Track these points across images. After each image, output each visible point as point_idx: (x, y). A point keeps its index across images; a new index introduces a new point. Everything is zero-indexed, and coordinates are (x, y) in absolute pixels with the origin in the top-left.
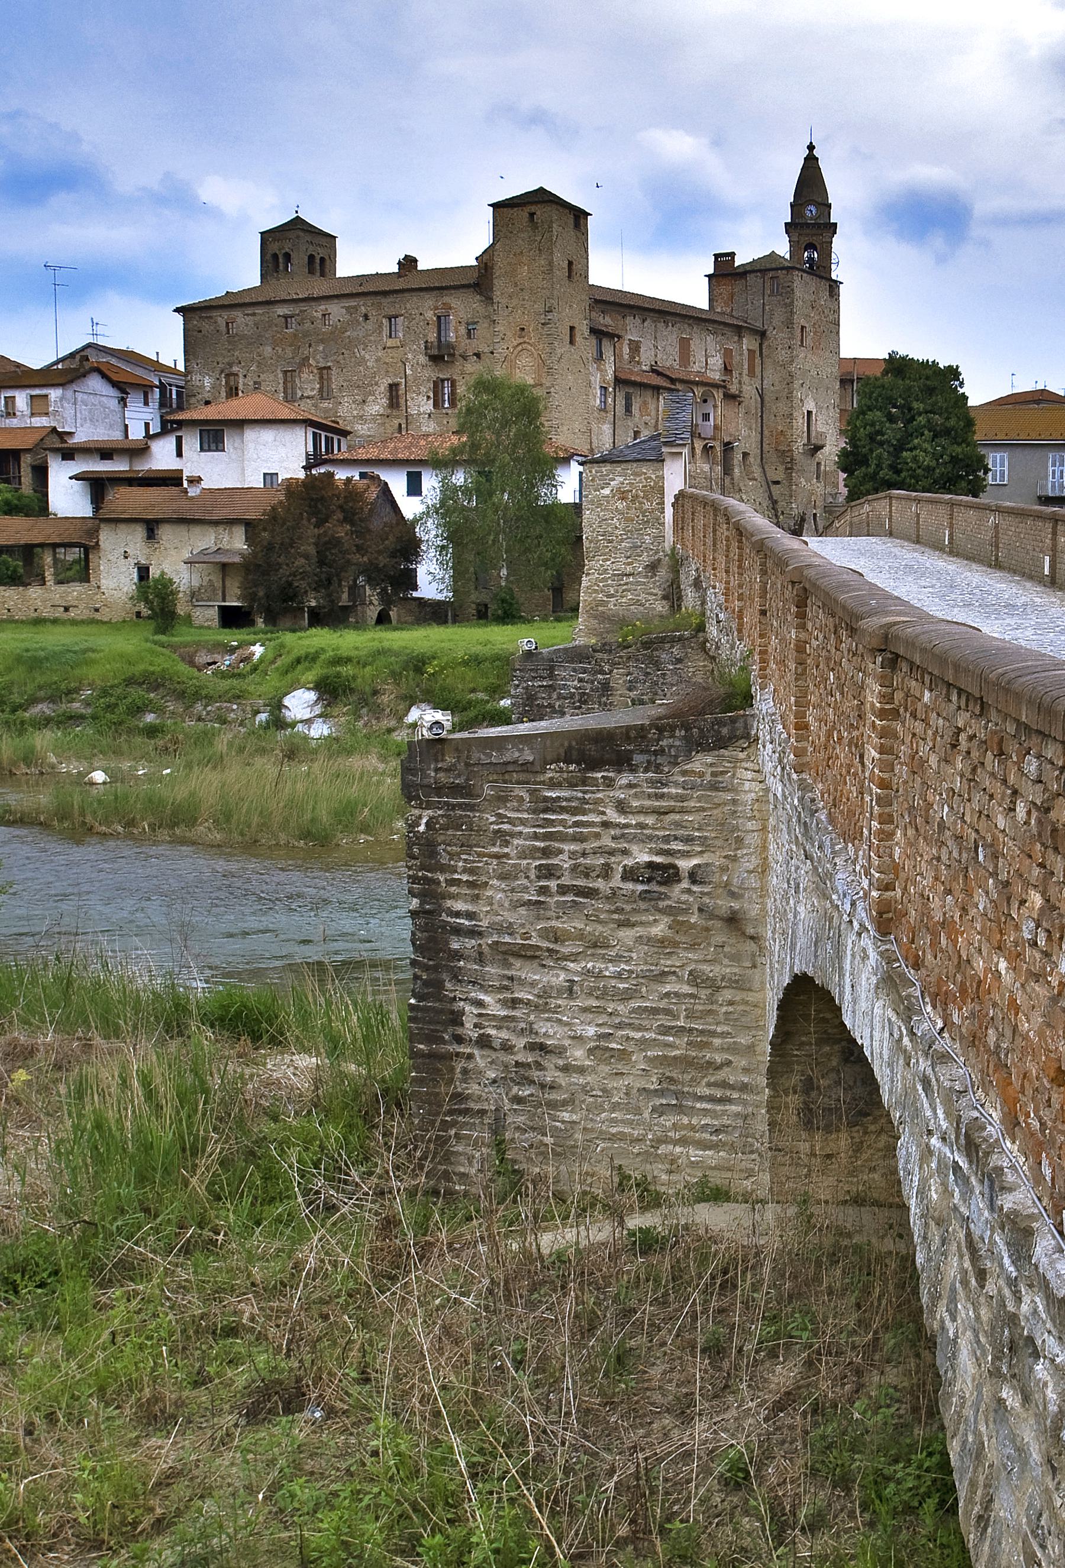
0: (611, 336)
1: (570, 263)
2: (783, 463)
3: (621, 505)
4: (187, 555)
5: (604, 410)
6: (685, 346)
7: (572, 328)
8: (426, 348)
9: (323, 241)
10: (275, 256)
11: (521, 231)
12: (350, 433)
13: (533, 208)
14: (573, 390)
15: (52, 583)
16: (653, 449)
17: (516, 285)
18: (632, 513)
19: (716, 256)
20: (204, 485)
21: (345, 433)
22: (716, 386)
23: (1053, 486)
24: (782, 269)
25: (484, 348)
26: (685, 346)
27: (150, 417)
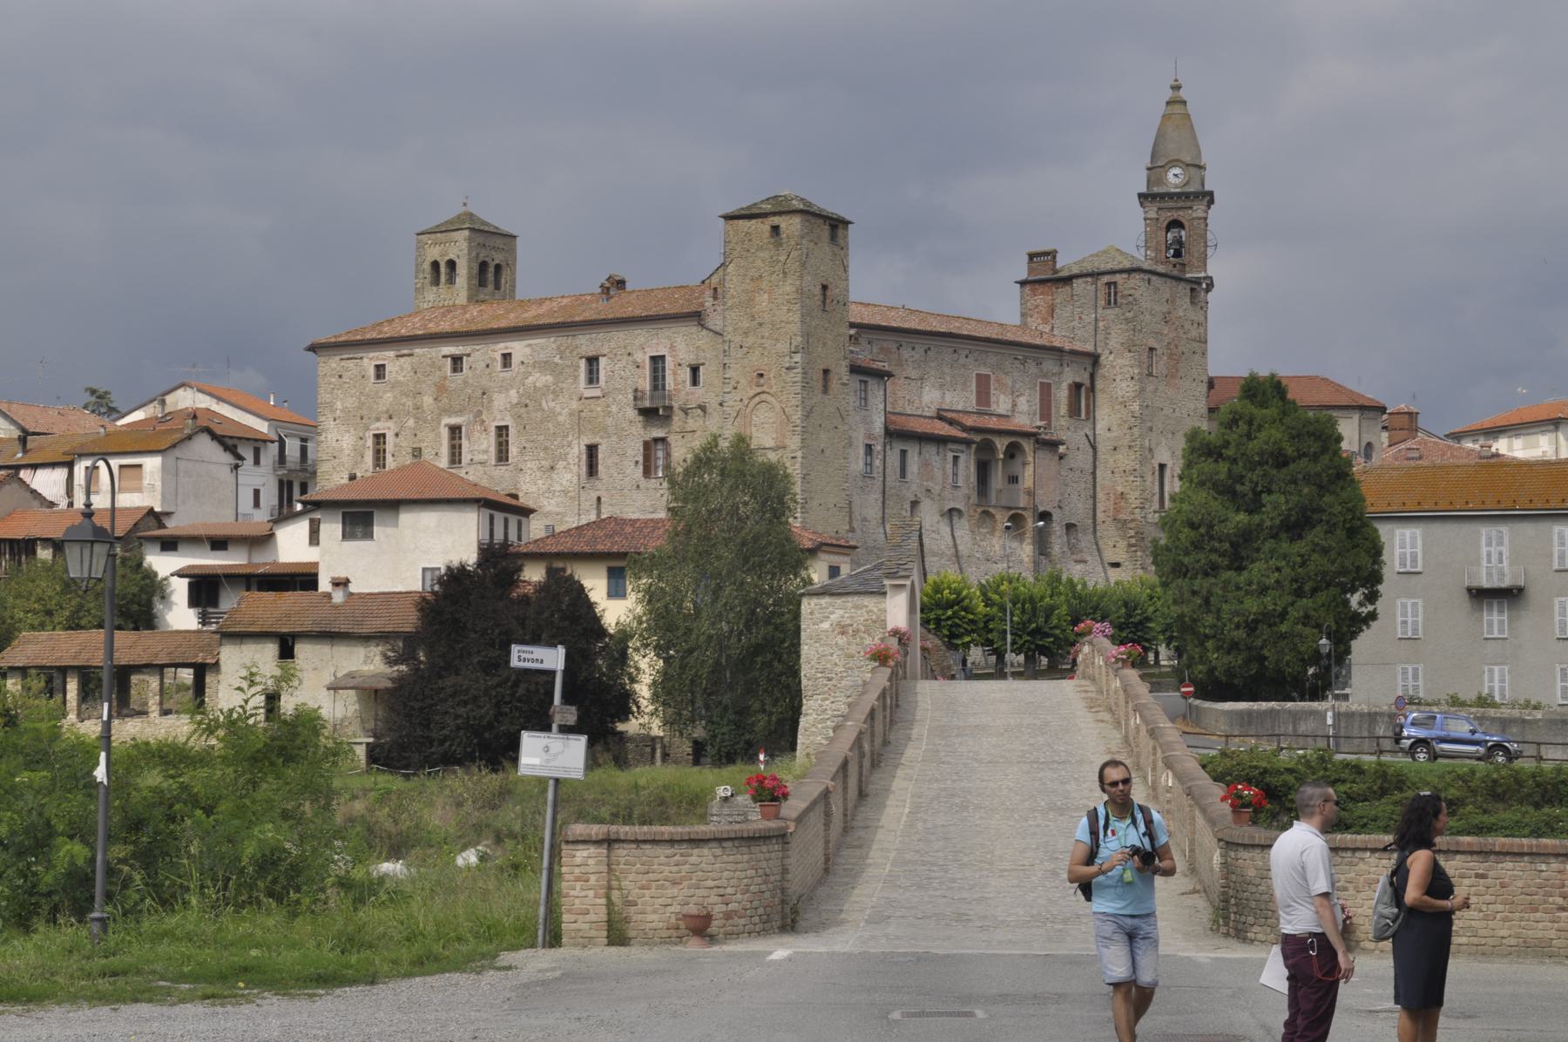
0: (882, 375)
1: (825, 287)
2: (1123, 537)
3: (841, 640)
4: (328, 678)
5: (867, 475)
6: (983, 384)
7: (826, 372)
8: (635, 398)
9: (499, 242)
10: (435, 265)
11: (760, 248)
12: (532, 511)
13: (776, 220)
14: (827, 453)
15: (156, 714)
16: (877, 579)
17: (753, 318)
18: (853, 649)
19: (1031, 256)
20: (353, 588)
21: (526, 512)
22: (1027, 435)
23: (1489, 574)
24: (1121, 271)
25: (712, 401)
26: (983, 384)
27: (264, 480)
